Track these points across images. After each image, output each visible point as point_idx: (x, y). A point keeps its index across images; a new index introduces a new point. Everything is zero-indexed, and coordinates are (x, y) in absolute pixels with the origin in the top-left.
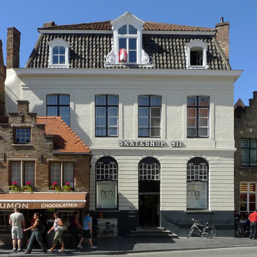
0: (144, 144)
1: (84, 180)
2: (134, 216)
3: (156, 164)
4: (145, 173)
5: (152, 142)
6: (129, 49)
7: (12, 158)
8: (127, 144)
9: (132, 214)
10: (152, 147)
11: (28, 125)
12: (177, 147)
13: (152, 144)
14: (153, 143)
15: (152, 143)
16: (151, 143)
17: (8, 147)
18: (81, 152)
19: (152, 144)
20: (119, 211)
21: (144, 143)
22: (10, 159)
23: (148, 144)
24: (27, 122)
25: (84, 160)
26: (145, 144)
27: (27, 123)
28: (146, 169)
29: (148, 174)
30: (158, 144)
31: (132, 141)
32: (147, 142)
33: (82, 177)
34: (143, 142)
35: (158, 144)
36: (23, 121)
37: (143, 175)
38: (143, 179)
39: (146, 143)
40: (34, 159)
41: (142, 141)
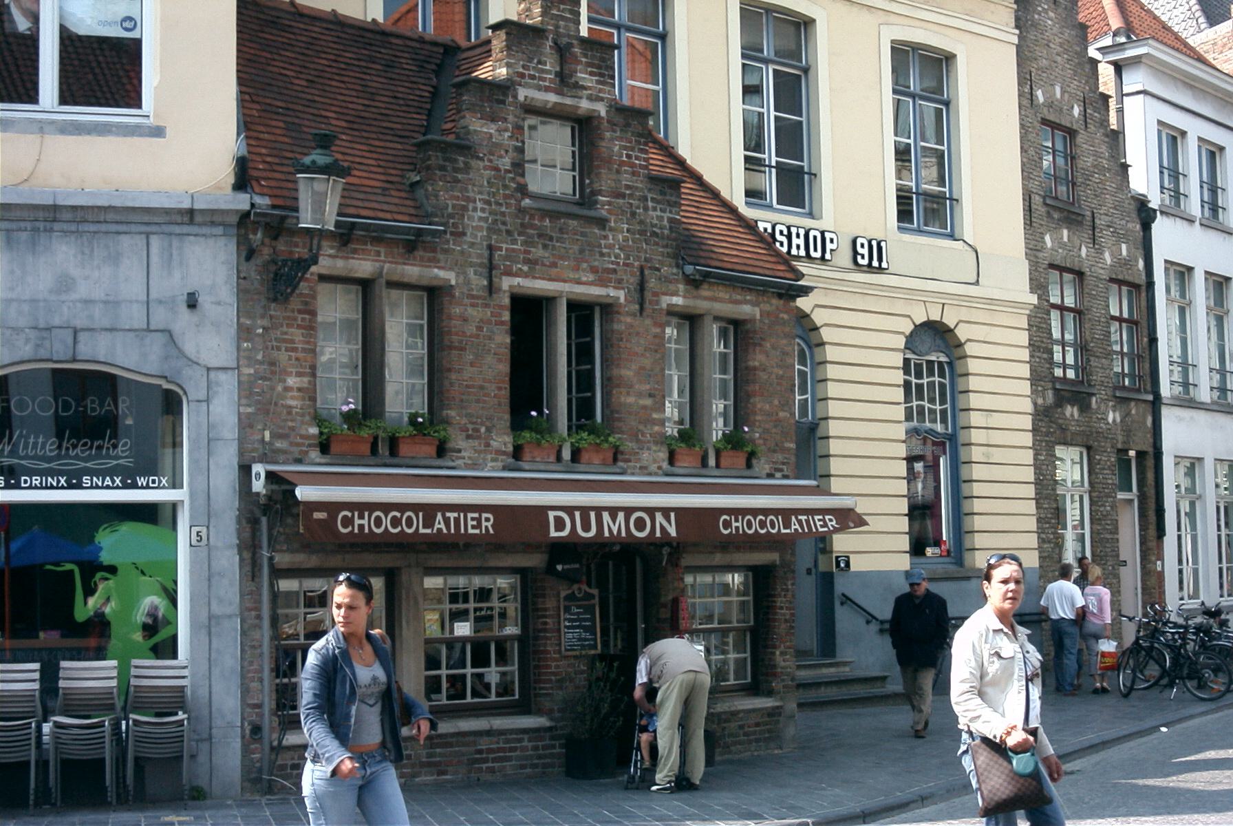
7: (526, 276)
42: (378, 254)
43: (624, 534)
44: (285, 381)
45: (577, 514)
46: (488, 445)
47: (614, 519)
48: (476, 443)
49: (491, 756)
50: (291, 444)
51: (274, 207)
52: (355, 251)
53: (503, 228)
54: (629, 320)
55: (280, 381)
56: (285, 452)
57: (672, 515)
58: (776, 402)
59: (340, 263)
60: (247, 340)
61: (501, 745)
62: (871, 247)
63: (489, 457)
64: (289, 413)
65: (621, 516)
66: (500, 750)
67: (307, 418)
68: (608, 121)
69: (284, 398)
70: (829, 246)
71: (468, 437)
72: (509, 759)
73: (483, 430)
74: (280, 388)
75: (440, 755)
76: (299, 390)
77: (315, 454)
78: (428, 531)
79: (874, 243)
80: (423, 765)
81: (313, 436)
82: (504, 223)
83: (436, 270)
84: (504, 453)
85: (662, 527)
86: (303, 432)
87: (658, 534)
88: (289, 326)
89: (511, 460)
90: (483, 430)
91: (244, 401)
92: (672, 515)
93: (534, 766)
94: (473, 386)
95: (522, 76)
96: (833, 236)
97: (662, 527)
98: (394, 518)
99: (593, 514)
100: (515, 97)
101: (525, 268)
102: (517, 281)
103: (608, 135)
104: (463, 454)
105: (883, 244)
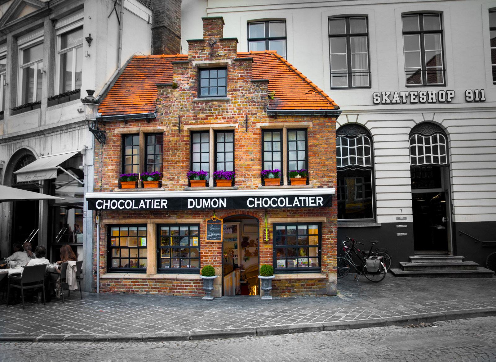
0: (417, 99)
1: (327, 163)
2: (405, 234)
3: (439, 135)
4: (421, 153)
5: (432, 94)
6: (207, 185)
7: (194, 124)
8: (387, 99)
9: (402, 230)
10: (432, 103)
11: (222, 61)
12: (477, 101)
13: (432, 99)
14: (434, 96)
15: (432, 96)
16: (430, 96)
17: (186, 105)
18: (320, 108)
19: (432, 99)
20: (379, 226)
21: (418, 96)
22: (190, 126)
23: (425, 97)
24: (221, 56)
25: (326, 124)
26: (420, 98)
27: (219, 58)
28: (422, 144)
29: (426, 154)
30: (442, 98)
31: (396, 95)
32: (423, 94)
33: (324, 158)
34: (416, 94)
35: (442, 98)
36: (212, 55)
37: (417, 156)
38: (432, 163)
39: (421, 96)
40: (232, 125)
41: (414, 93)
42: (138, 124)
43: (209, 207)
44: (108, 167)
45: (196, 200)
46: (178, 182)
47: (207, 201)
48: (173, 182)
49: (178, 287)
50: (109, 186)
51: (102, 116)
52: (131, 125)
53: (186, 109)
54: (240, 134)
55: (106, 167)
56: (107, 189)
57: (225, 199)
58: (324, 158)
59: (125, 129)
60: (97, 156)
61: (182, 284)
62: (475, 93)
63: (178, 186)
64: (109, 177)
65: (209, 200)
66: (181, 286)
67: (114, 178)
68: (232, 65)
69: (107, 172)
70: (450, 96)
71: (170, 180)
72: (185, 289)
73: (176, 177)
74: (106, 169)
75: (159, 285)
76: (112, 170)
77: (116, 189)
78: (137, 208)
79: (477, 92)
80: (153, 288)
81: (116, 183)
82: (186, 108)
83: (159, 127)
84: (184, 185)
85: (221, 204)
86: (113, 182)
87: (220, 207)
88: (109, 151)
89: (187, 187)
90: (176, 177)
91: (96, 174)
92: (225, 199)
93: (194, 292)
94: (172, 163)
95: (195, 57)
96: (451, 92)
97: (221, 204)
98: (121, 203)
99: (201, 200)
100: (192, 65)
101: (194, 122)
102: (190, 126)
103: (232, 70)
104: (168, 186)
105: (482, 91)
